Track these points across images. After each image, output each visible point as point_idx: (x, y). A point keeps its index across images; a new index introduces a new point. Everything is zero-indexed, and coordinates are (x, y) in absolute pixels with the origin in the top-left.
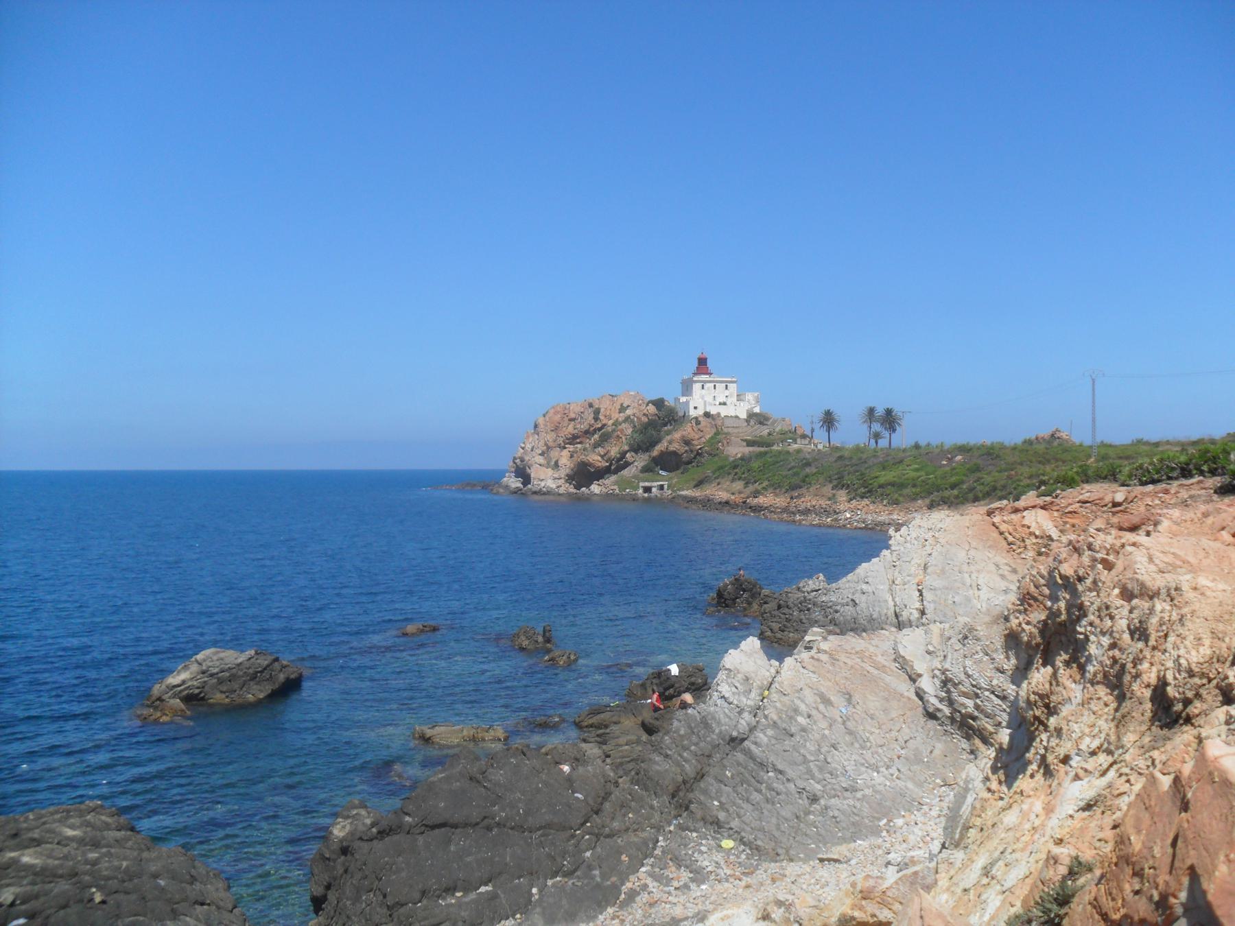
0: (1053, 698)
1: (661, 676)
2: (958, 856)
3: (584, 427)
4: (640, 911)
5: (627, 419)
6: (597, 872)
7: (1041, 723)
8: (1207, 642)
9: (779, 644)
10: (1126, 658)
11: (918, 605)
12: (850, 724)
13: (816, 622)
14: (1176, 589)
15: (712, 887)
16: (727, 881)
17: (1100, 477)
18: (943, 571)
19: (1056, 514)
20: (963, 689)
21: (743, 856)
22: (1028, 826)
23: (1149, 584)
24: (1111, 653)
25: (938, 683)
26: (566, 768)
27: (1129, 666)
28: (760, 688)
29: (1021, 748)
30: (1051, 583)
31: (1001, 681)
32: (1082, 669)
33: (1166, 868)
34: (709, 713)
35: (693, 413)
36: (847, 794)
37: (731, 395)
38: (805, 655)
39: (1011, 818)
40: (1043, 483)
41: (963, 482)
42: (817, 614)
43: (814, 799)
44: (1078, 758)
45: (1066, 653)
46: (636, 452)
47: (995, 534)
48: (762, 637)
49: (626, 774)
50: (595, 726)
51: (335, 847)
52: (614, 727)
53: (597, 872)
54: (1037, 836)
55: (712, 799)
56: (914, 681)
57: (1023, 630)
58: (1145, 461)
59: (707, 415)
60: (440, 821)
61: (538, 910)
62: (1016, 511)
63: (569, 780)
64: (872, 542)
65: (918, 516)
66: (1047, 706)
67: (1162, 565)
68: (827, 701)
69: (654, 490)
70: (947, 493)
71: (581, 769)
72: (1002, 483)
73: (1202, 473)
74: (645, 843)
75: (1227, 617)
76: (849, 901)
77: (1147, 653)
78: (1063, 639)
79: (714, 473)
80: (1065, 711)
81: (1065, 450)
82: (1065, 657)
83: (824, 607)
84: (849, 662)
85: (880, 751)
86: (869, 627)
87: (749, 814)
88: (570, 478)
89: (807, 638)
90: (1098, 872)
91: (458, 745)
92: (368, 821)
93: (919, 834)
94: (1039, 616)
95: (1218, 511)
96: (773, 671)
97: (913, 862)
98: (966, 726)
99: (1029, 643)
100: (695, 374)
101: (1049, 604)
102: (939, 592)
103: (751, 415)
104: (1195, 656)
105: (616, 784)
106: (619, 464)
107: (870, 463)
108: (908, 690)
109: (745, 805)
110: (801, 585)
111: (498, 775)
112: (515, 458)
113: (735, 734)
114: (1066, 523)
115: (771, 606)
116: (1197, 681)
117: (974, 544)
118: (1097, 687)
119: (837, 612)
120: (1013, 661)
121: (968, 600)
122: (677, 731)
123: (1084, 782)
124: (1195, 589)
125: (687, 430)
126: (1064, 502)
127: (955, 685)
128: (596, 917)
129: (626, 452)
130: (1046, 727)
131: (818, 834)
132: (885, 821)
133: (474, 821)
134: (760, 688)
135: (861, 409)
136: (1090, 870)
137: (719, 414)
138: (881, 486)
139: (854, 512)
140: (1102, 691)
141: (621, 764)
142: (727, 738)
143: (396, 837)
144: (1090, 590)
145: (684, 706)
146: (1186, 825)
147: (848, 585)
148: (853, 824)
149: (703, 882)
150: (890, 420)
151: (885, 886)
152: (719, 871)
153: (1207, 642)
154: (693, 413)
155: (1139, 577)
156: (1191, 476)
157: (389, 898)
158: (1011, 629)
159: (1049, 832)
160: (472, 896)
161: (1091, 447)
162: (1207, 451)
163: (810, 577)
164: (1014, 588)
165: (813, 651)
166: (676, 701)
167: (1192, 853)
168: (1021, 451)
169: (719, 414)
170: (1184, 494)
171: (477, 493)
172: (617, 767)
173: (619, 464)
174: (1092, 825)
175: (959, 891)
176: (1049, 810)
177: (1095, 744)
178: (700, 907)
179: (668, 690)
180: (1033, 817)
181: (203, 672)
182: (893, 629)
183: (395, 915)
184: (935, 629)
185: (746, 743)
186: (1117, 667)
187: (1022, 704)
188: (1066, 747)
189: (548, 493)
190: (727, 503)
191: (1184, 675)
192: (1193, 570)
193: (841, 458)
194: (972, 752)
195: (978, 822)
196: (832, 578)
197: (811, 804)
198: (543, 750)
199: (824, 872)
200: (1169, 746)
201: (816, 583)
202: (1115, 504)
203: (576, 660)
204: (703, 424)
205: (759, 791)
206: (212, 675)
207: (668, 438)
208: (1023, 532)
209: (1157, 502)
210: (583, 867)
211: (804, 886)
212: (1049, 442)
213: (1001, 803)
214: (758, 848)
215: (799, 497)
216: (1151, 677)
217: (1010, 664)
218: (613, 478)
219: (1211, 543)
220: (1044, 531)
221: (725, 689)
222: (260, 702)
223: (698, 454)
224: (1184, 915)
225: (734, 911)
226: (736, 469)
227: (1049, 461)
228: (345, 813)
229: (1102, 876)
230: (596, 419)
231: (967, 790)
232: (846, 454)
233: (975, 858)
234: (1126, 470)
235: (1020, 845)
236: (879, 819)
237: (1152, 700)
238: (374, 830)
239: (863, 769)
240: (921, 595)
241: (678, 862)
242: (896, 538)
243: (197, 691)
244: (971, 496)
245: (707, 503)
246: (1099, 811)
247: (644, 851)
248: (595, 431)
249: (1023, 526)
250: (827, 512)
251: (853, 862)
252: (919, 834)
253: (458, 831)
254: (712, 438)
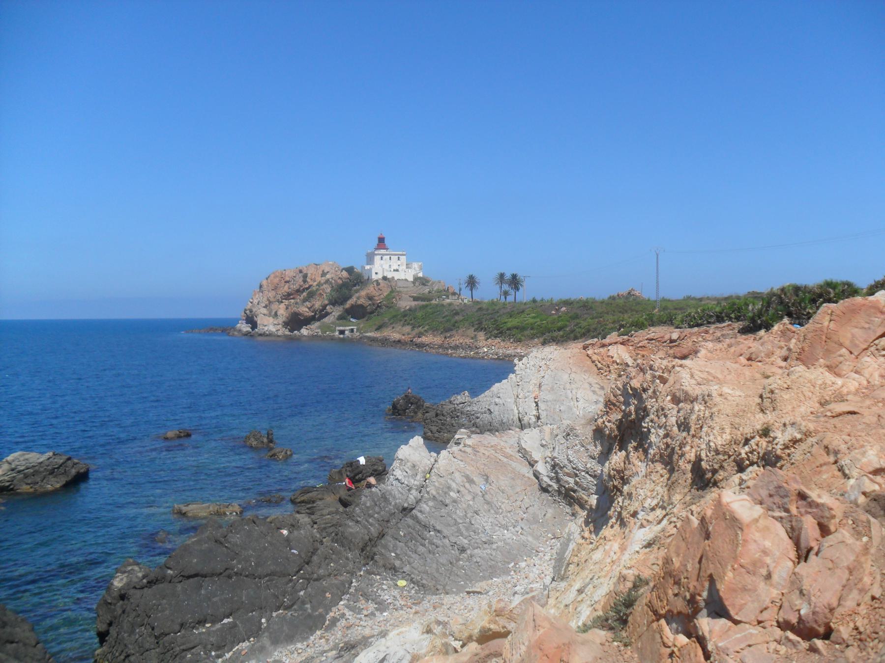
0: (626, 472)
1: (353, 464)
2: (563, 584)
3: (296, 287)
4: (340, 633)
5: (327, 281)
6: (308, 606)
7: (618, 490)
8: (728, 431)
9: (437, 441)
10: (675, 444)
11: (535, 412)
12: (487, 497)
13: (463, 425)
14: (708, 396)
15: (391, 614)
16: (402, 609)
17: (661, 322)
18: (552, 389)
19: (631, 348)
20: (567, 471)
21: (413, 592)
22: (609, 560)
23: (690, 392)
24: (665, 441)
25: (549, 467)
26: (285, 532)
27: (677, 448)
28: (424, 472)
29: (603, 507)
30: (625, 393)
31: (592, 465)
32: (646, 452)
33: (694, 577)
34: (387, 491)
35: (374, 277)
36: (486, 546)
37: (402, 264)
38: (455, 449)
39: (597, 555)
40: (622, 326)
41: (566, 326)
42: (464, 420)
43: (463, 550)
44: (643, 513)
45: (635, 441)
47: (589, 362)
48: (425, 438)
49: (329, 535)
50: (305, 502)
51: (116, 594)
52: (319, 503)
53: (308, 606)
54: (614, 567)
55: (390, 551)
56: (532, 466)
57: (606, 426)
58: (692, 311)
59: (385, 278)
60: (193, 573)
61: (266, 634)
62: (603, 346)
63: (287, 540)
64: (503, 368)
65: (534, 350)
66: (622, 478)
67: (699, 380)
68: (471, 481)
69: (347, 332)
70: (555, 334)
71: (296, 532)
72: (594, 326)
73: (730, 319)
74: (343, 583)
75: (741, 414)
76: (487, 618)
77: (689, 440)
78: (633, 432)
79: (389, 320)
80: (634, 481)
81: (638, 304)
82: (634, 444)
83: (469, 415)
84: (487, 453)
85: (509, 515)
86: (500, 428)
87: (417, 562)
88: (286, 324)
89: (457, 437)
90: (652, 584)
91: (205, 518)
92: (140, 575)
93: (537, 571)
94: (617, 416)
95: (738, 343)
96: (432, 460)
97: (532, 590)
98: (569, 496)
99: (610, 434)
100: (376, 249)
101: (623, 407)
102: (549, 403)
103: (416, 279)
104: (720, 440)
105: (322, 543)
106: (322, 314)
107: (501, 312)
108: (527, 472)
109: (414, 556)
110: (452, 399)
111: (236, 539)
112: (246, 310)
113: (406, 505)
114: (638, 354)
115: (431, 414)
116: (721, 457)
117: (574, 369)
118: (655, 464)
119: (478, 418)
120: (599, 448)
121: (570, 408)
122: (365, 504)
123: (647, 529)
124: (721, 395)
125: (370, 290)
126: (636, 340)
127: (561, 468)
128: (308, 638)
129: (326, 305)
130: (621, 492)
131: (466, 574)
132: (513, 564)
133: (218, 571)
134: (424, 472)
135: (495, 274)
136: (647, 584)
137: (393, 278)
138: (509, 329)
139: (490, 348)
140: (659, 467)
141: (325, 528)
142: (401, 508)
143: (161, 586)
144: (651, 398)
145: (369, 486)
146: (708, 548)
147: (485, 399)
148: (490, 567)
149: (385, 611)
150: (515, 282)
151: (512, 606)
152: (396, 602)
153: (728, 431)
154: (374, 277)
155: (684, 388)
156: (724, 321)
157: (156, 630)
158: (598, 426)
159: (623, 563)
160: (218, 626)
161: (656, 301)
162: (734, 304)
163: (458, 394)
164: (602, 400)
165: (462, 445)
166: (364, 483)
167: (711, 566)
168: (608, 304)
169: (393, 278)
170: (718, 334)
171: (214, 339)
172: (321, 530)
173: (322, 314)
174: (652, 557)
175: (562, 606)
176: (623, 548)
177: (655, 502)
178: (383, 628)
179: (357, 475)
180: (612, 554)
181: (13, 470)
182: (518, 430)
183: (161, 642)
184: (547, 429)
185: (414, 511)
186: (669, 450)
187: (605, 478)
188: (634, 506)
189: (270, 335)
190: (399, 341)
191: (713, 453)
192: (720, 382)
193: (480, 309)
194: (573, 515)
195: (576, 559)
196: (474, 393)
197: (460, 554)
198: (268, 520)
199: (471, 601)
200: (702, 501)
201: (463, 397)
202: (672, 341)
203: (291, 455)
204: (382, 285)
205: (424, 545)
206: (19, 472)
207: (357, 295)
208: (609, 361)
209: (700, 339)
210: (299, 603)
211: (457, 611)
212: (627, 298)
213: (591, 546)
214: (423, 586)
215: (450, 337)
216: (691, 456)
217: (597, 450)
218: (317, 324)
219: (733, 365)
220: (623, 360)
221: (398, 473)
222: (55, 492)
223: (378, 306)
224: (705, 607)
225: (407, 628)
226: (407, 317)
227: (626, 311)
228: (123, 569)
229: (655, 586)
230: (305, 281)
231: (569, 540)
232: (484, 306)
233: (573, 583)
234: (679, 317)
235: (603, 573)
236: (509, 563)
237: (692, 471)
238: (145, 581)
239: (497, 528)
240: (537, 405)
241: (367, 597)
242: (519, 365)
243: (7, 484)
244: (572, 335)
245: (385, 342)
246: (656, 547)
247: (342, 590)
248: (304, 290)
249: (608, 356)
250: (470, 348)
251: (491, 593)
252: (537, 571)
253: (207, 579)
254: (388, 295)
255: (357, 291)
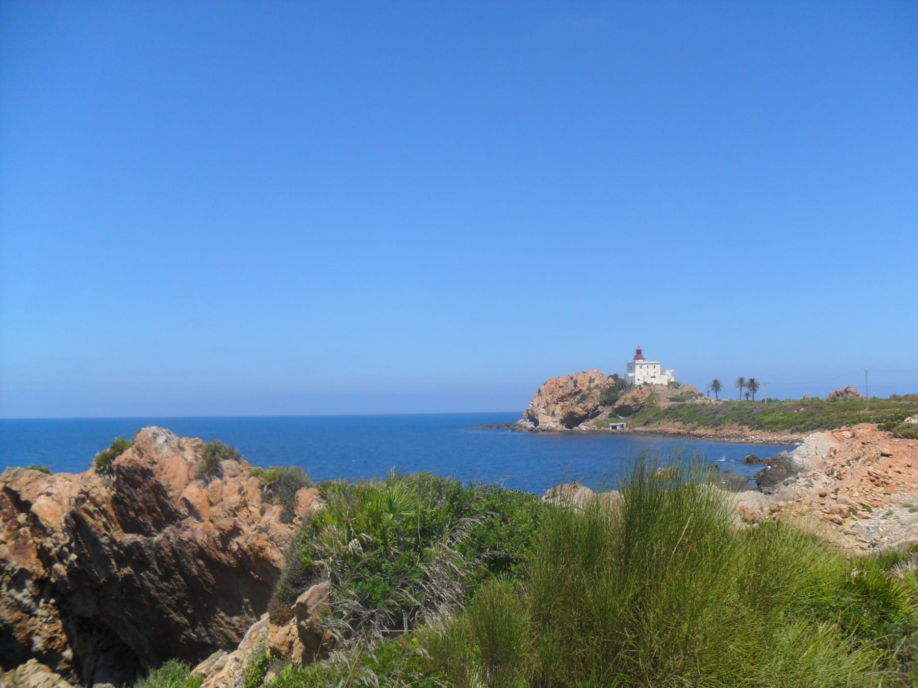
3: (568, 391)
5: (597, 386)
35: (637, 383)
46: (604, 405)
59: (645, 384)
70: (799, 426)
81: (854, 405)
88: (562, 422)
103: (670, 383)
106: (594, 413)
125: (635, 393)
139: (786, 436)
154: (637, 383)
173: (594, 413)
189: (551, 430)
193: (734, 409)
207: (624, 397)
218: (592, 421)
226: (671, 414)
230: (575, 386)
245: (665, 434)
255: (623, 394)
